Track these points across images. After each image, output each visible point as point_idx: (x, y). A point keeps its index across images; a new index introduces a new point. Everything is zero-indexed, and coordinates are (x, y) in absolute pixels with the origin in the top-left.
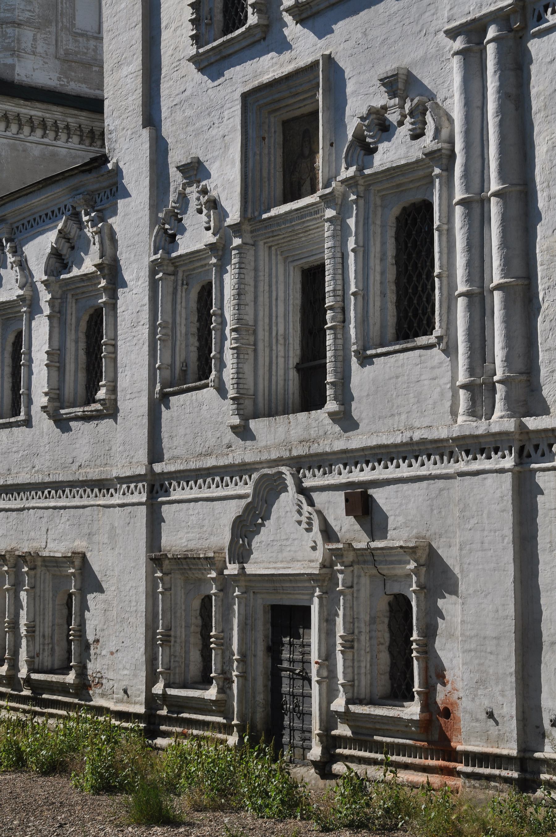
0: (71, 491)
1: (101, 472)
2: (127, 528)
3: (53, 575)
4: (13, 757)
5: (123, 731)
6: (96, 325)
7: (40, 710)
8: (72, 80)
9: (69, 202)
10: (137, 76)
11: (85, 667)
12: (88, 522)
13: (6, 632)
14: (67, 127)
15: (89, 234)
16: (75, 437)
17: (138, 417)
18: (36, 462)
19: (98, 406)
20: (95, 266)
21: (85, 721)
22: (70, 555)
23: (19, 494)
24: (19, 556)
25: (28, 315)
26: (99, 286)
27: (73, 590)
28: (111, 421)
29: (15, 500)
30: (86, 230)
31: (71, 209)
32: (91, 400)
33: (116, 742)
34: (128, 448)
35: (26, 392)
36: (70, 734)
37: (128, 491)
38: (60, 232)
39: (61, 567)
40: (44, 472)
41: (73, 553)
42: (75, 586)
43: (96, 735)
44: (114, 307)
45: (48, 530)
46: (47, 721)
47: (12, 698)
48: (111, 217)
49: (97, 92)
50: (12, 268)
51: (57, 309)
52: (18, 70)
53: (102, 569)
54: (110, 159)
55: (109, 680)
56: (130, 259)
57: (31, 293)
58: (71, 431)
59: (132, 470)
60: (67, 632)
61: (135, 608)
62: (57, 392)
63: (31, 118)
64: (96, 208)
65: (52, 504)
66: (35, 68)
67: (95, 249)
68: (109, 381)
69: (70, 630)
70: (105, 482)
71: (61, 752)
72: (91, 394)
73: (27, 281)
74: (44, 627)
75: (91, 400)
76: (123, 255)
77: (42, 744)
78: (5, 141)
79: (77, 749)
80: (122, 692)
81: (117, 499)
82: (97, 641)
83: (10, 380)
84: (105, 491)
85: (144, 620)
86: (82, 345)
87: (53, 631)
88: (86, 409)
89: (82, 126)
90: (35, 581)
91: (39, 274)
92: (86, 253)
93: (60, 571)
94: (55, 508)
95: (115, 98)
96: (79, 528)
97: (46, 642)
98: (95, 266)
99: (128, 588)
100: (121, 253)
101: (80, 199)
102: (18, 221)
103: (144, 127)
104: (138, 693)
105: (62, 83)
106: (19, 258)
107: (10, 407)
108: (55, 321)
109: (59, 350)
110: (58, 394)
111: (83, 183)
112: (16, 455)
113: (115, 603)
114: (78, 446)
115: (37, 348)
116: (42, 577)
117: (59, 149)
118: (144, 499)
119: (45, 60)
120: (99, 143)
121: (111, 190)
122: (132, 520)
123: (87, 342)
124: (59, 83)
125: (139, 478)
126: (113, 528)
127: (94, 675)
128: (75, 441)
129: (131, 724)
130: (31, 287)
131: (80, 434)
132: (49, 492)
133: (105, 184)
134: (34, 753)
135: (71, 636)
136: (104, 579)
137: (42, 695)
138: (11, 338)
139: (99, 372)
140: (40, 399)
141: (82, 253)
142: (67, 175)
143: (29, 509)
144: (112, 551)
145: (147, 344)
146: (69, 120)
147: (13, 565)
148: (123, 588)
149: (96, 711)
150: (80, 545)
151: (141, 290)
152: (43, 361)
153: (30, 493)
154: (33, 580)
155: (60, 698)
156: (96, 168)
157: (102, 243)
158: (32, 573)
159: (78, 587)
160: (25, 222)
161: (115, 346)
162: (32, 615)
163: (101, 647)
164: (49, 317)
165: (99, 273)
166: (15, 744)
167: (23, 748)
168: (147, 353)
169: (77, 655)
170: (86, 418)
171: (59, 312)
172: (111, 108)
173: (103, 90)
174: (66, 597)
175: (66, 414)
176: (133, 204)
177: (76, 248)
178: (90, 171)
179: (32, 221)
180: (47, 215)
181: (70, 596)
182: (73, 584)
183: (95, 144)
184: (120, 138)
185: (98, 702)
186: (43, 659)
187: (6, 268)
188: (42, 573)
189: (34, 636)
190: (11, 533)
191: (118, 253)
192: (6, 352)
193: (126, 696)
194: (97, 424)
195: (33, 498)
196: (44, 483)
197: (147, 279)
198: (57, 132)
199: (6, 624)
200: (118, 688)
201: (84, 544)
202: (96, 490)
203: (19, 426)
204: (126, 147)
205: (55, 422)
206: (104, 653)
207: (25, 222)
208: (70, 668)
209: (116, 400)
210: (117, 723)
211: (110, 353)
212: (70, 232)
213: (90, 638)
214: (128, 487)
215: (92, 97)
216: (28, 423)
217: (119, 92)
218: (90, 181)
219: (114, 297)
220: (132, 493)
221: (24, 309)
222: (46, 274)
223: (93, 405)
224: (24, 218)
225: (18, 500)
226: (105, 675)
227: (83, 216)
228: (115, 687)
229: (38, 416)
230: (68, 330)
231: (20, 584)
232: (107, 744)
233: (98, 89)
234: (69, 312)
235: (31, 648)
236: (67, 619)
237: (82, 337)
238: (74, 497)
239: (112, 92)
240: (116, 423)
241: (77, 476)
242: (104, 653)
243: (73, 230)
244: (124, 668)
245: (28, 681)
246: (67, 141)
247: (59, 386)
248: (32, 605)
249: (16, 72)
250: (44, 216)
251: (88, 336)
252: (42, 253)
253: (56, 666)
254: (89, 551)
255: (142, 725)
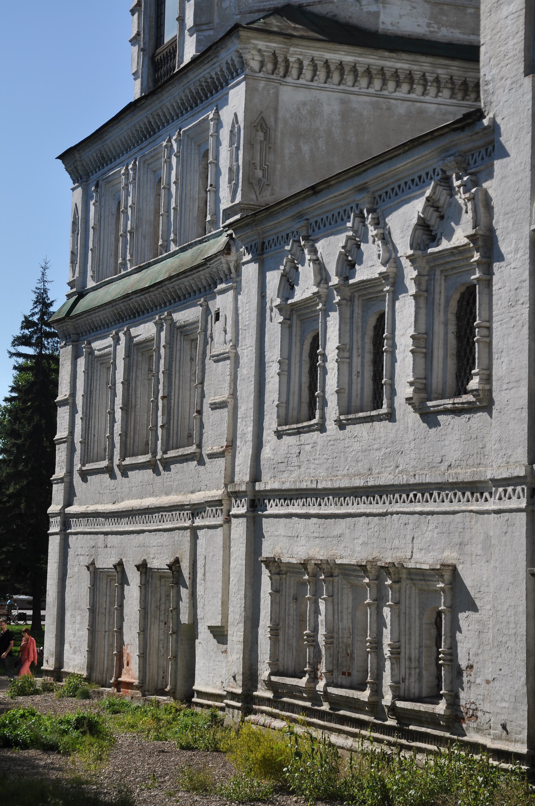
0: (439, 494)
1: (474, 473)
2: (504, 538)
3: (420, 590)
4: (378, 795)
5: (503, 773)
6: (468, 305)
7: (407, 743)
8: (443, 25)
9: (439, 166)
10: (519, 16)
11: (457, 697)
12: (459, 530)
13: (368, 652)
14: (437, 80)
15: (461, 201)
16: (444, 433)
17: (517, 409)
18: (400, 460)
19: (470, 398)
20: (468, 237)
21: (459, 758)
22: (438, 567)
23: (381, 497)
24: (382, 567)
25: (391, 294)
26: (472, 260)
27: (442, 608)
28: (485, 415)
29: (377, 503)
30: (457, 197)
31: (440, 173)
32: (462, 390)
33: (495, 786)
34: (504, 446)
35: (389, 382)
36: (442, 772)
37: (505, 495)
38: (428, 199)
39: (428, 580)
40: (409, 472)
41: (442, 565)
42: (444, 603)
43: (471, 775)
44: (489, 284)
45: (413, 538)
46: (415, 756)
47: (375, 728)
48: (486, 181)
49: (472, 37)
50: (374, 242)
51: (424, 287)
52: (382, 18)
53: (476, 584)
54: (486, 114)
55: (484, 713)
56: (507, 228)
57: (394, 270)
58: (440, 425)
59: (510, 471)
60: (435, 654)
61: (514, 631)
62: (424, 381)
63: (396, 72)
64: (469, 171)
65: (418, 509)
66: (402, 14)
67: (467, 218)
68: (483, 369)
69: (439, 653)
70: (479, 485)
71: (432, 793)
72: (463, 384)
73: (391, 257)
74: (410, 649)
75: (462, 390)
76: (500, 224)
77: (410, 782)
78: (367, 99)
79: (450, 790)
80: (500, 727)
81: (491, 505)
82: (471, 667)
83: (371, 368)
84: (478, 494)
85: (525, 645)
86: (452, 328)
87: (420, 653)
88: (457, 400)
89: (454, 78)
90: (400, 596)
91: (404, 249)
92: (457, 223)
93: (428, 585)
94: (421, 513)
95: (492, 43)
96: (448, 536)
97: (413, 666)
98: (468, 237)
99: (505, 607)
100: (497, 222)
101: (450, 162)
102: (381, 189)
103: (526, 74)
104: (519, 729)
105: (432, 29)
106: (381, 231)
107: (371, 398)
108: (422, 301)
109: (426, 334)
110: (425, 384)
111: (454, 143)
112: (377, 453)
113: (491, 624)
114: (447, 443)
115: (402, 332)
116: (408, 592)
117: (428, 105)
118: (523, 505)
119: (413, 4)
120: (473, 96)
121: (487, 150)
122: (510, 529)
123: (457, 325)
124: (428, 29)
125: (518, 481)
126: (488, 537)
127: (468, 706)
128: (443, 437)
129: (511, 766)
130: (395, 262)
131: (449, 430)
132: (415, 496)
133: (480, 143)
134: (401, 791)
135: (440, 659)
136: (478, 595)
137: (408, 726)
138: (372, 321)
139: (471, 359)
140: (404, 390)
141: (453, 224)
142: (436, 134)
143: (392, 514)
144: (487, 564)
145: (527, 326)
146: (440, 71)
147: (375, 577)
148: (500, 607)
149: (471, 748)
150: (450, 556)
151: (520, 264)
152: (408, 346)
153: (394, 496)
154: (397, 595)
155: (429, 731)
156: (469, 125)
157: (475, 211)
158: (396, 586)
159: (448, 604)
160: (389, 189)
161: (489, 329)
162: (397, 635)
163: (475, 674)
164: (415, 297)
165: (472, 245)
166: (380, 780)
167: (389, 786)
168: (527, 336)
169: (448, 681)
170: (456, 411)
171: (426, 291)
172: (488, 55)
173: (479, 35)
174: (434, 615)
175: (434, 406)
176: (512, 164)
177: (446, 217)
178: (462, 129)
179: (397, 188)
180: (413, 181)
181: (439, 614)
182: (443, 600)
183: (468, 98)
184: (498, 89)
185: (472, 737)
186: (409, 685)
187: (367, 242)
188: (408, 587)
189: (399, 658)
190: (373, 540)
191: (494, 221)
192: (366, 337)
193: (505, 733)
194: (469, 419)
195: (397, 502)
196: (409, 485)
197: (528, 251)
198: (425, 86)
199: (368, 644)
200: (496, 722)
201: (455, 555)
202: (468, 494)
203: (381, 420)
204: (505, 99)
205: (421, 415)
206: (478, 681)
207: (389, 189)
208: (441, 697)
209: (490, 391)
210: (495, 763)
211: (484, 337)
212: (439, 200)
213: (463, 663)
214: (505, 491)
215: (465, 43)
216: (391, 417)
217: (498, 36)
218: (463, 141)
219: (489, 272)
220: (510, 498)
221: (387, 288)
222: (411, 249)
223: (464, 396)
224: (388, 185)
225: (381, 503)
226: (480, 707)
227: (454, 180)
228: (492, 721)
229: (403, 409)
230: (435, 311)
231: (383, 599)
232: (485, 787)
233: (473, 34)
234: (437, 290)
235: (396, 672)
236: (436, 640)
237: (452, 318)
238: (443, 501)
239: (489, 37)
240: (491, 417)
241: (446, 477)
242: (478, 681)
243: (443, 197)
244: (503, 700)
245: (393, 710)
246: (437, 96)
247: (426, 374)
248: (397, 624)
249: (381, 20)
250: (410, 183)
251: (459, 317)
252: (407, 224)
253: (424, 694)
254: (460, 563)
255: (524, 768)
